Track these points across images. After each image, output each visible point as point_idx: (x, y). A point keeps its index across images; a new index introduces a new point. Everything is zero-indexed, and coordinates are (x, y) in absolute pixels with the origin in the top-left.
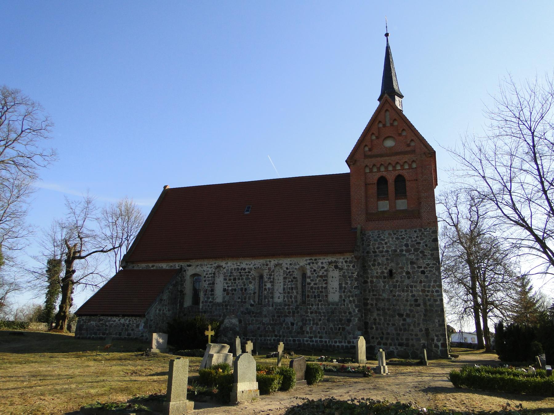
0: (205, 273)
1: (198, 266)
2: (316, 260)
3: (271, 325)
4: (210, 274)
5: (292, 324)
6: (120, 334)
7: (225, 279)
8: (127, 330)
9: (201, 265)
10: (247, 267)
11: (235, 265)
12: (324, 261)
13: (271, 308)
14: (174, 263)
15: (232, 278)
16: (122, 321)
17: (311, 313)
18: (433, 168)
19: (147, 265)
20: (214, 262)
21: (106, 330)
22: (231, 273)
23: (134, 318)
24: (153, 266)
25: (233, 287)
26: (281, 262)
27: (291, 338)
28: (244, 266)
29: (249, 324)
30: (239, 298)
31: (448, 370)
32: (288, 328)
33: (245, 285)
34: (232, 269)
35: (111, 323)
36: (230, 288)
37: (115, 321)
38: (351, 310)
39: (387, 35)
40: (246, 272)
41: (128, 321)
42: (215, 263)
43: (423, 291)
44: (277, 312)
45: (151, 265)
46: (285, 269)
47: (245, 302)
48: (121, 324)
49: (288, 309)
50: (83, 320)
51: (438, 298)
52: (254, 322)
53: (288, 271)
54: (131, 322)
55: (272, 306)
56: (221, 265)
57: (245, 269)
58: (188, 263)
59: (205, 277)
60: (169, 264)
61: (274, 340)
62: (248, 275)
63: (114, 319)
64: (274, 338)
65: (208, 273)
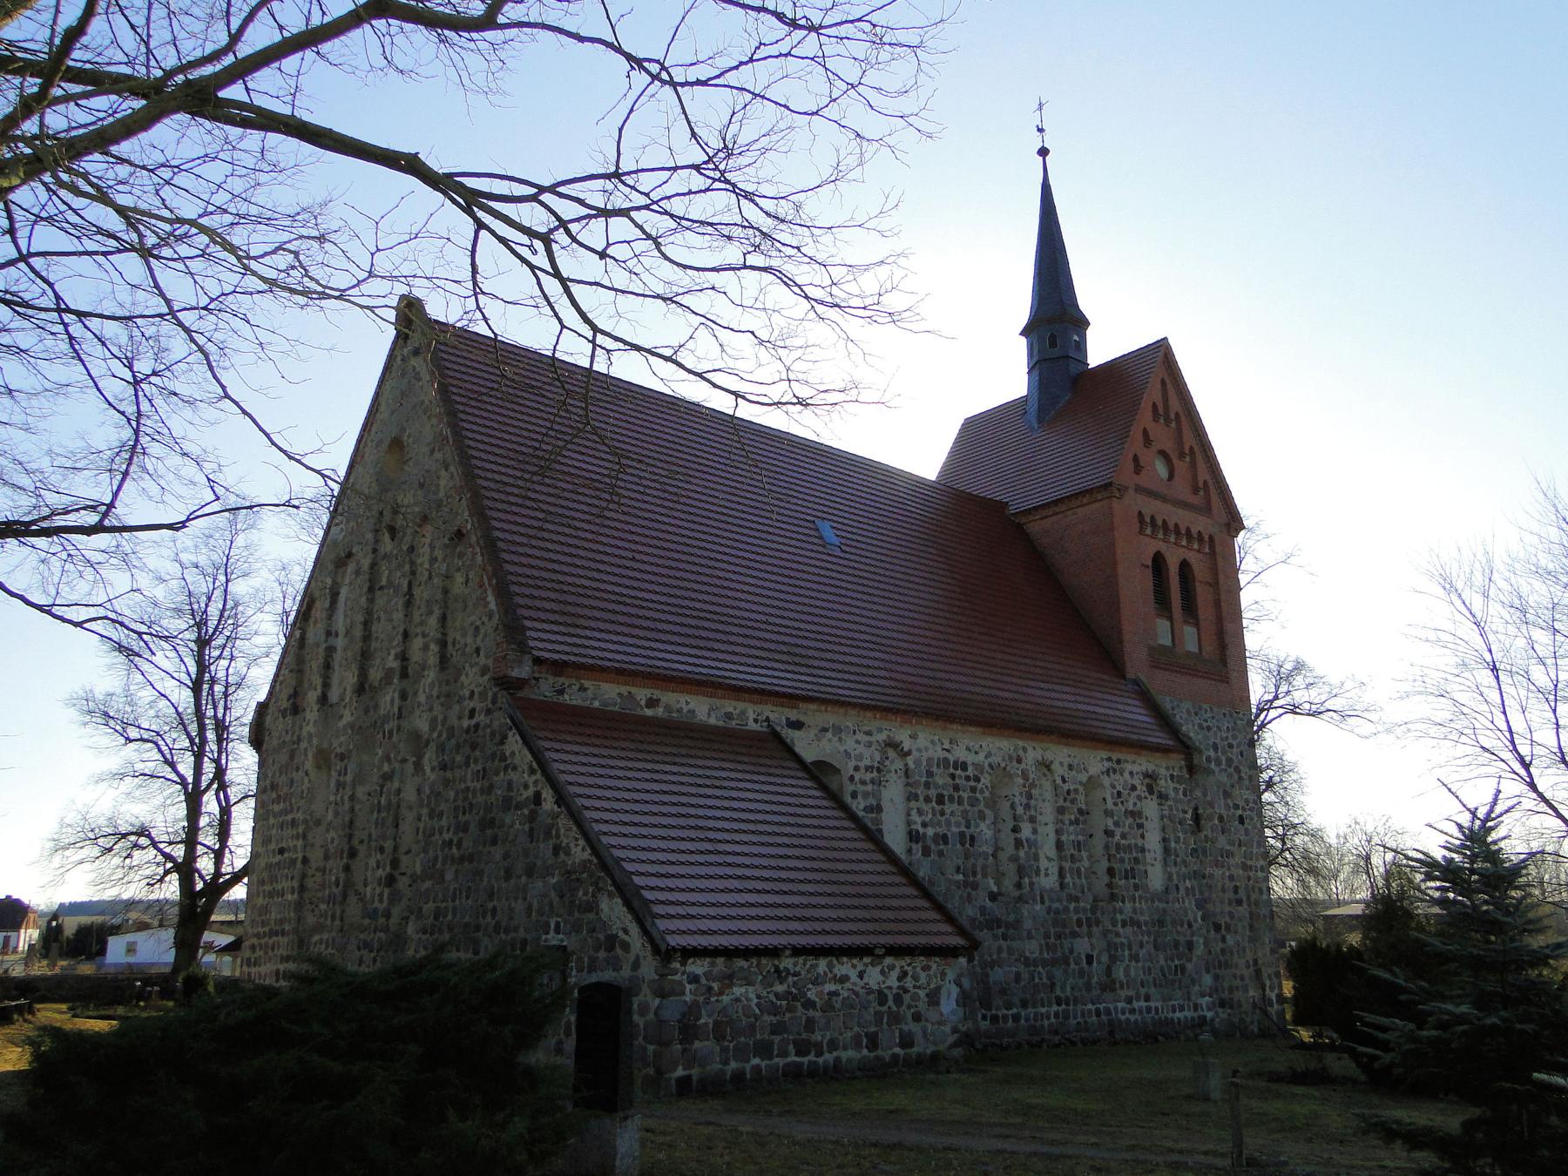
0: (852, 764)
1: (825, 730)
2: (1119, 762)
3: (1044, 963)
4: (867, 769)
5: (1090, 959)
6: (873, 1043)
7: (912, 797)
8: (896, 1018)
9: (838, 730)
10: (970, 759)
11: (939, 748)
12: (1136, 768)
13: (1038, 907)
14: (741, 706)
15: (933, 793)
16: (874, 977)
17: (1124, 924)
18: (359, 469)
19: (624, 690)
20: (878, 723)
21: (810, 1025)
22: (930, 774)
23: (920, 961)
24: (652, 703)
25: (939, 830)
26: (1049, 756)
27: (1090, 1006)
28: (960, 754)
29: (992, 965)
30: (958, 870)
31: (915, 1049)
32: (1082, 973)
33: (968, 827)
34: (929, 760)
35: (830, 987)
36: (930, 832)
37: (844, 979)
38: (1191, 916)
39: (1043, 152)
40: (968, 778)
41: (895, 974)
42: (880, 730)
43: (1245, 867)
44: (1056, 923)
45: (642, 694)
46: (1059, 781)
47: (975, 886)
48: (870, 991)
49: (1077, 910)
50: (694, 979)
51: (1264, 886)
52: (1004, 955)
53: (1066, 787)
54: (909, 983)
55: (1043, 902)
56: (898, 738)
57: (964, 767)
58: (793, 715)
59: (852, 778)
60: (718, 702)
61: (1056, 1015)
62: (973, 790)
63: (845, 968)
64: (1055, 1008)
65: (862, 765)
